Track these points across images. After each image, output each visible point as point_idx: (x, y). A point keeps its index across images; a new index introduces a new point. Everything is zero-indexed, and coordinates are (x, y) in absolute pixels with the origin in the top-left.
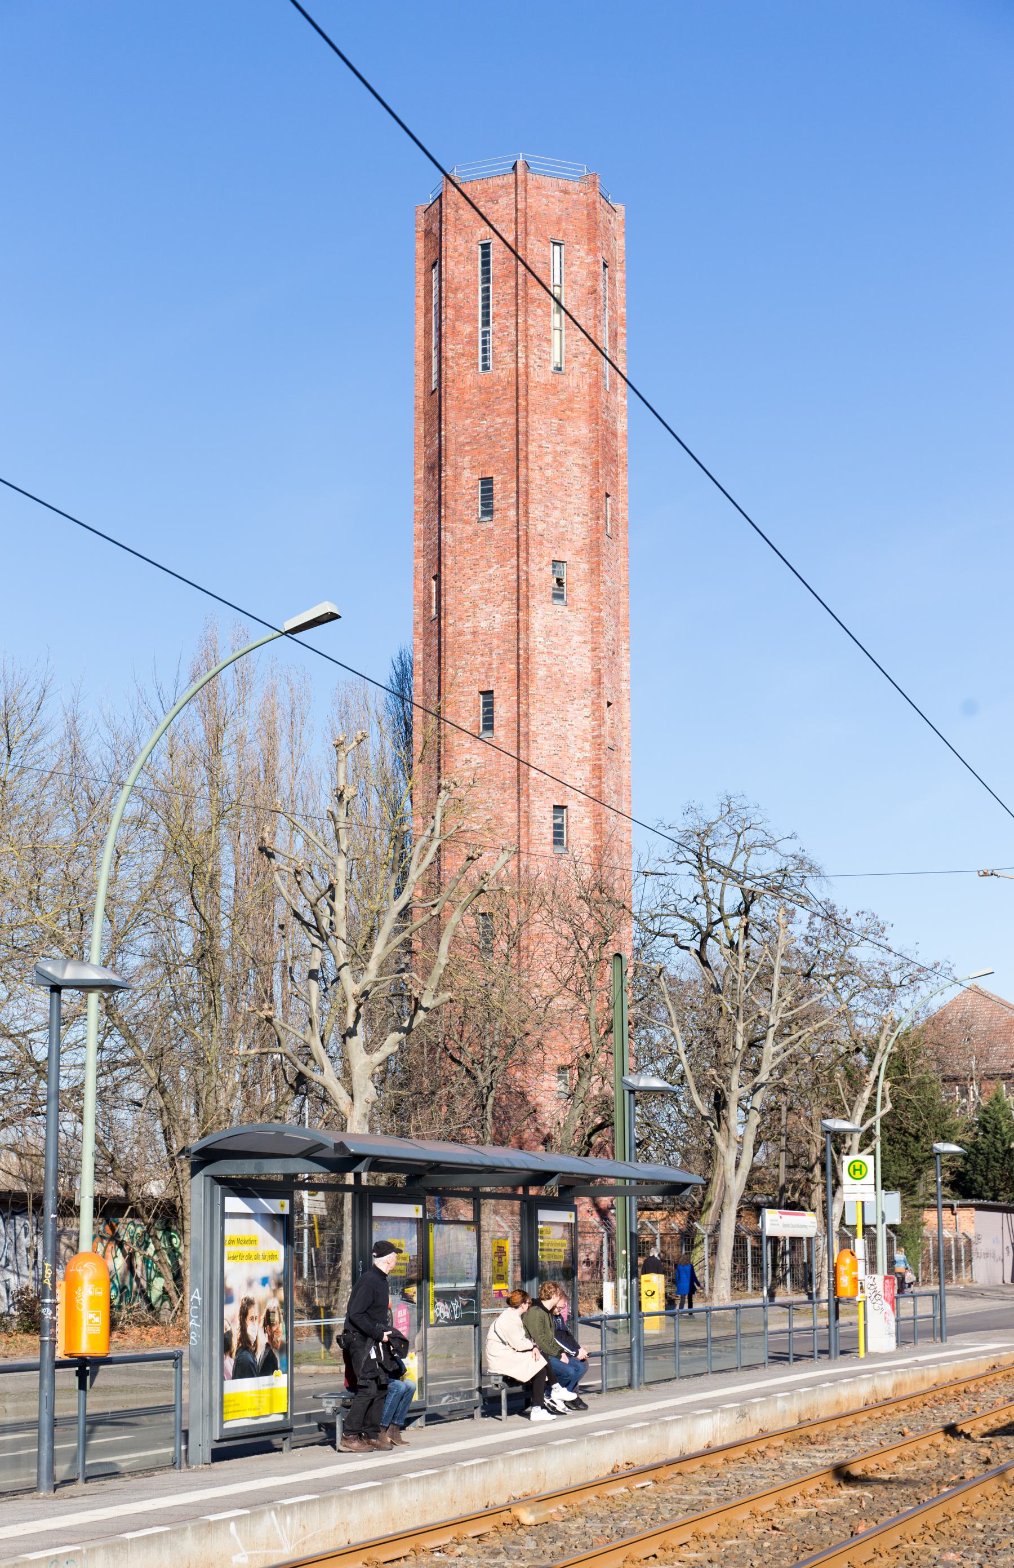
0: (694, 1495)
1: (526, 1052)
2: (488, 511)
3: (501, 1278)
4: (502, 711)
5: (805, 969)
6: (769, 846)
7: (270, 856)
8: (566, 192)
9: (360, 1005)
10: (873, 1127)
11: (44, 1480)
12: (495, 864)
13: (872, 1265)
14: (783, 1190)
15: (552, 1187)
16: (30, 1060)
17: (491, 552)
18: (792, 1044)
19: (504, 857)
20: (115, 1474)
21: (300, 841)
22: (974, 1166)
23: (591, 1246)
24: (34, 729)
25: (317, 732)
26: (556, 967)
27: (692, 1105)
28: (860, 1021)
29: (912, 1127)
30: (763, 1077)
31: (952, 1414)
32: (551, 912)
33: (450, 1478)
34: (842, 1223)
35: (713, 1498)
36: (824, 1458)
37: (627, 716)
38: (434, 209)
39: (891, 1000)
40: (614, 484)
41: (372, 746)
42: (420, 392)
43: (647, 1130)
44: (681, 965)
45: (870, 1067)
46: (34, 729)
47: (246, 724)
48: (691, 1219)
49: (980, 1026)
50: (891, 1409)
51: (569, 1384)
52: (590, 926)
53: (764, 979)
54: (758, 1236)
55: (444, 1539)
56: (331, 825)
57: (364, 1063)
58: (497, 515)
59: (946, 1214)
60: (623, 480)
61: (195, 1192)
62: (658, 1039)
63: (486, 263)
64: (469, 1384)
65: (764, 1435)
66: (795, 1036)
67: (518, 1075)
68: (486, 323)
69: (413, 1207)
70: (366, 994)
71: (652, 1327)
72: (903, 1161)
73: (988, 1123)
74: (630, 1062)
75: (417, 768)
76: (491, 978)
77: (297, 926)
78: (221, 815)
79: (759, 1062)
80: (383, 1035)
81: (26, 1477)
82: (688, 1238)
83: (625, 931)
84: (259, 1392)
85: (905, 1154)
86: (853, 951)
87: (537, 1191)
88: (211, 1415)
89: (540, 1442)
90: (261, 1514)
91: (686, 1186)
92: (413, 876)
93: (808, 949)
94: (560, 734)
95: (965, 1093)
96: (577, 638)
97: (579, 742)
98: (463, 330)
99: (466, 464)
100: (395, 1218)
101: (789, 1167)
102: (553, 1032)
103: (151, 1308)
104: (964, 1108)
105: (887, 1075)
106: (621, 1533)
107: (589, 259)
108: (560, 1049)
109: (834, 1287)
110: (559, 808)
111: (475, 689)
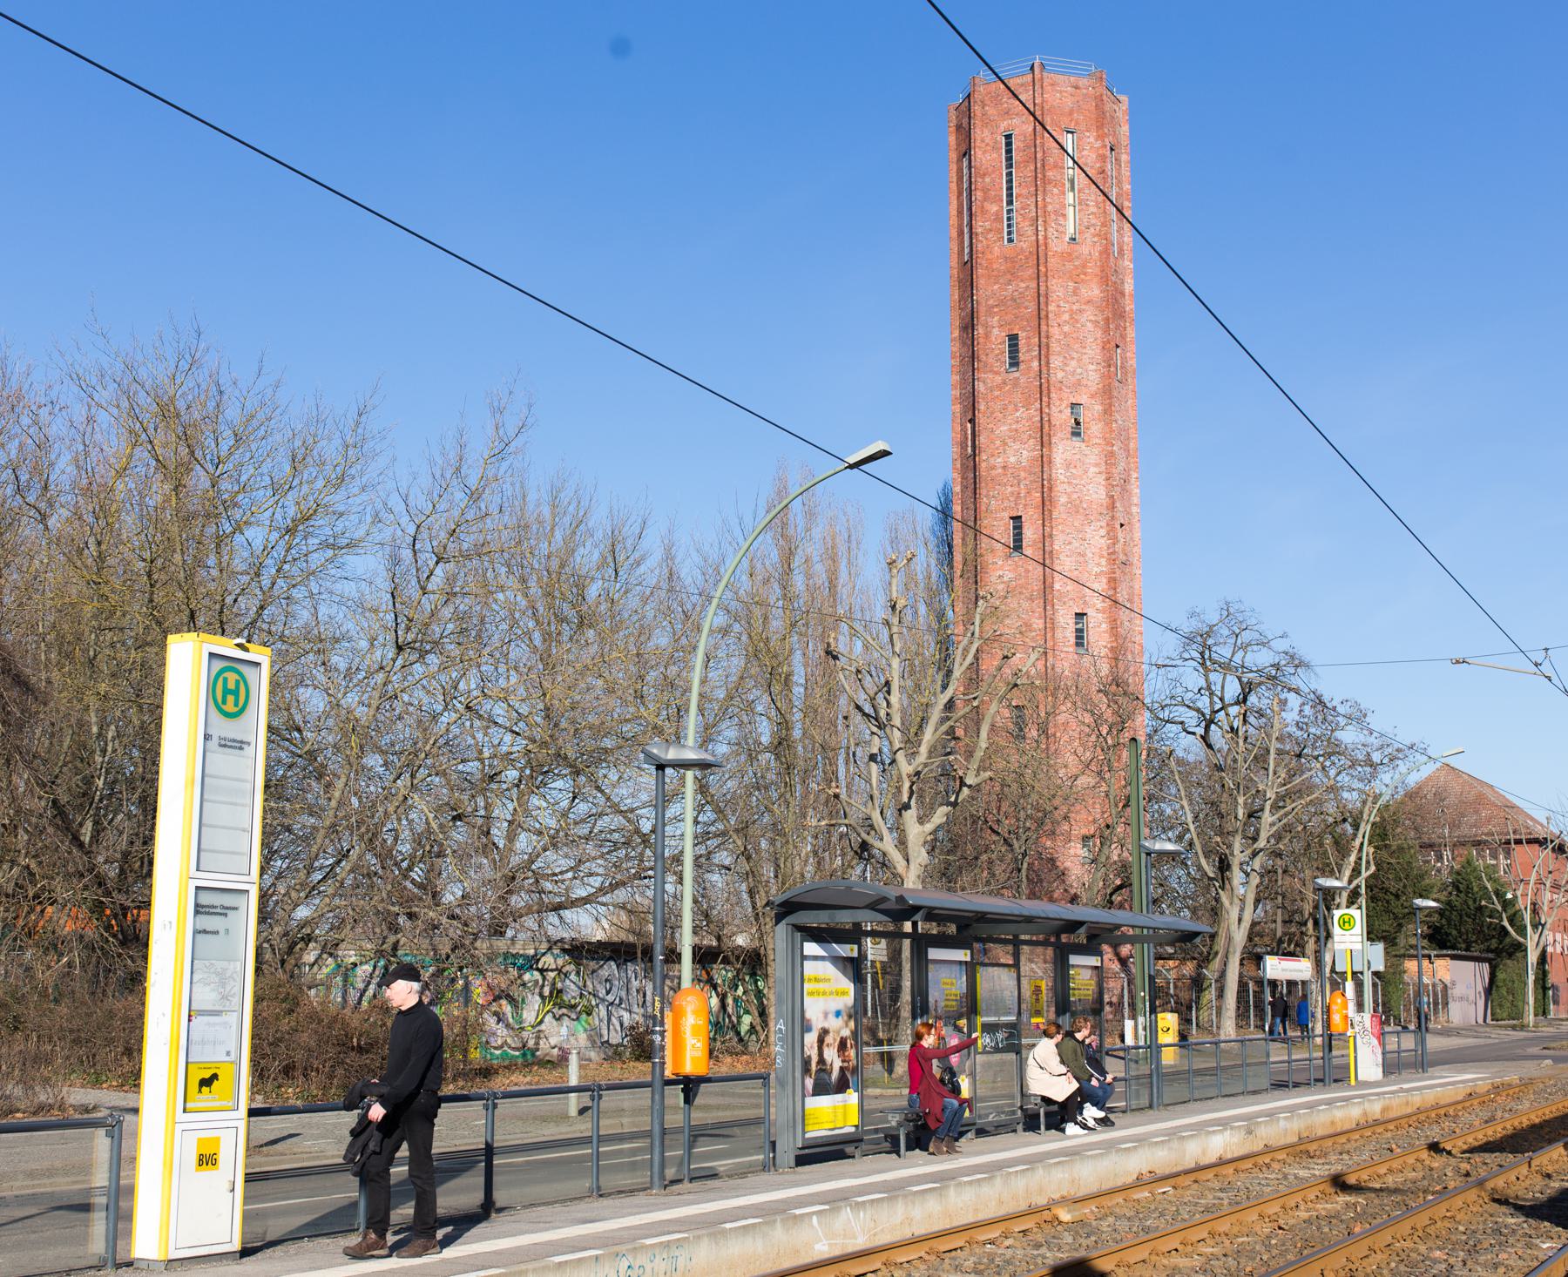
0: (1209, 1199)
1: (1055, 823)
2: (1015, 362)
3: (1038, 1013)
4: (1029, 534)
5: (1297, 750)
6: (1263, 644)
7: (835, 658)
8: (1077, 87)
9: (913, 783)
10: (1358, 886)
11: (656, 1179)
12: (1027, 662)
13: (1360, 1007)
14: (1280, 941)
15: (1081, 936)
16: (637, 831)
17: (1017, 397)
18: (1286, 815)
19: (1034, 656)
20: (713, 1175)
21: (859, 644)
22: (1449, 920)
23: (1115, 987)
24: (637, 555)
25: (874, 545)
26: (1080, 751)
27: (1200, 868)
28: (1346, 795)
29: (1393, 886)
30: (1261, 843)
31: (1434, 1133)
32: (1074, 703)
33: (998, 1181)
34: (1333, 970)
35: (1226, 1202)
36: (1321, 1170)
37: (1137, 535)
38: (964, 108)
39: (1373, 776)
40: (1123, 337)
41: (919, 566)
42: (955, 263)
43: (1160, 891)
44: (1188, 747)
45: (1355, 835)
46: (637, 555)
47: (811, 549)
48: (1200, 966)
49: (1452, 800)
50: (1380, 1129)
51: (1098, 1104)
52: (1108, 715)
53: (1261, 759)
54: (1260, 982)
55: (994, 1233)
56: (886, 631)
57: (917, 832)
58: (1022, 366)
59: (1425, 963)
60: (1131, 333)
61: (779, 938)
62: (1169, 811)
63: (1009, 151)
64: (1013, 1105)
65: (1268, 1150)
66: (1289, 808)
67: (1049, 843)
68: (1010, 202)
69: (962, 952)
70: (918, 773)
71: (1169, 1057)
72: (1385, 917)
73: (1461, 883)
74: (1145, 831)
75: (958, 582)
76: (1024, 759)
77: (859, 717)
78: (793, 625)
79: (1257, 831)
80: (932, 810)
81: (642, 1178)
82: (1198, 983)
83: (1139, 719)
84: (835, 1108)
85: (1387, 911)
86: (1338, 734)
87: (1068, 938)
88: (794, 1126)
89: (1075, 1153)
90: (838, 1209)
91: (1197, 934)
92: (957, 673)
93: (1299, 733)
94: (1080, 549)
95: (1440, 858)
96: (1093, 470)
97: (1097, 559)
98: (991, 209)
99: (995, 324)
100: (947, 972)
101: (1284, 922)
102: (1078, 807)
103: (741, 1040)
104: (1439, 871)
105: (1370, 843)
106: (1146, 1230)
107: (1098, 144)
108: (1084, 821)
109: (1327, 1024)
110: (1080, 616)
111: (1006, 515)
